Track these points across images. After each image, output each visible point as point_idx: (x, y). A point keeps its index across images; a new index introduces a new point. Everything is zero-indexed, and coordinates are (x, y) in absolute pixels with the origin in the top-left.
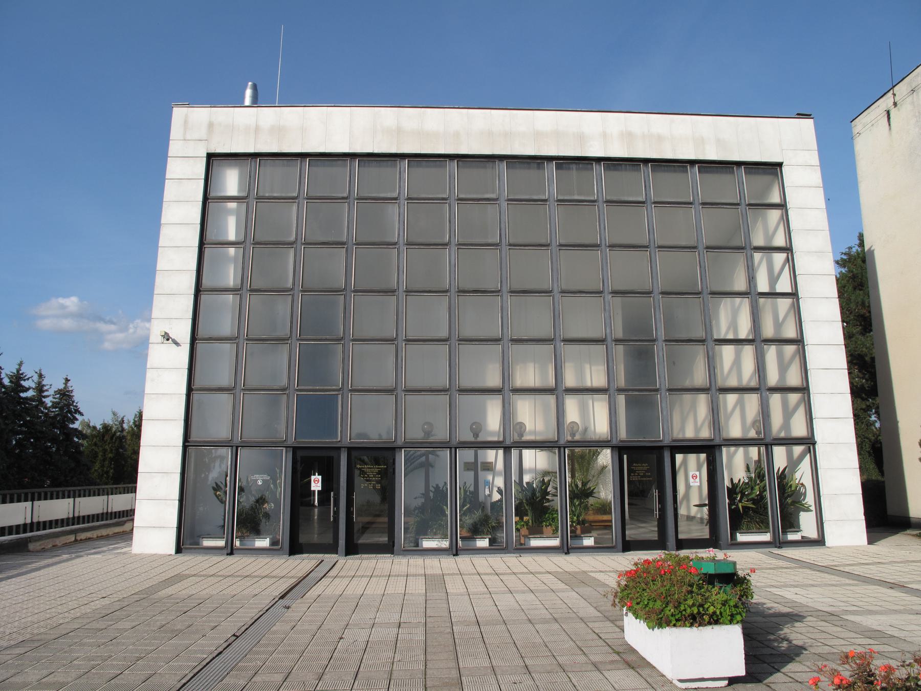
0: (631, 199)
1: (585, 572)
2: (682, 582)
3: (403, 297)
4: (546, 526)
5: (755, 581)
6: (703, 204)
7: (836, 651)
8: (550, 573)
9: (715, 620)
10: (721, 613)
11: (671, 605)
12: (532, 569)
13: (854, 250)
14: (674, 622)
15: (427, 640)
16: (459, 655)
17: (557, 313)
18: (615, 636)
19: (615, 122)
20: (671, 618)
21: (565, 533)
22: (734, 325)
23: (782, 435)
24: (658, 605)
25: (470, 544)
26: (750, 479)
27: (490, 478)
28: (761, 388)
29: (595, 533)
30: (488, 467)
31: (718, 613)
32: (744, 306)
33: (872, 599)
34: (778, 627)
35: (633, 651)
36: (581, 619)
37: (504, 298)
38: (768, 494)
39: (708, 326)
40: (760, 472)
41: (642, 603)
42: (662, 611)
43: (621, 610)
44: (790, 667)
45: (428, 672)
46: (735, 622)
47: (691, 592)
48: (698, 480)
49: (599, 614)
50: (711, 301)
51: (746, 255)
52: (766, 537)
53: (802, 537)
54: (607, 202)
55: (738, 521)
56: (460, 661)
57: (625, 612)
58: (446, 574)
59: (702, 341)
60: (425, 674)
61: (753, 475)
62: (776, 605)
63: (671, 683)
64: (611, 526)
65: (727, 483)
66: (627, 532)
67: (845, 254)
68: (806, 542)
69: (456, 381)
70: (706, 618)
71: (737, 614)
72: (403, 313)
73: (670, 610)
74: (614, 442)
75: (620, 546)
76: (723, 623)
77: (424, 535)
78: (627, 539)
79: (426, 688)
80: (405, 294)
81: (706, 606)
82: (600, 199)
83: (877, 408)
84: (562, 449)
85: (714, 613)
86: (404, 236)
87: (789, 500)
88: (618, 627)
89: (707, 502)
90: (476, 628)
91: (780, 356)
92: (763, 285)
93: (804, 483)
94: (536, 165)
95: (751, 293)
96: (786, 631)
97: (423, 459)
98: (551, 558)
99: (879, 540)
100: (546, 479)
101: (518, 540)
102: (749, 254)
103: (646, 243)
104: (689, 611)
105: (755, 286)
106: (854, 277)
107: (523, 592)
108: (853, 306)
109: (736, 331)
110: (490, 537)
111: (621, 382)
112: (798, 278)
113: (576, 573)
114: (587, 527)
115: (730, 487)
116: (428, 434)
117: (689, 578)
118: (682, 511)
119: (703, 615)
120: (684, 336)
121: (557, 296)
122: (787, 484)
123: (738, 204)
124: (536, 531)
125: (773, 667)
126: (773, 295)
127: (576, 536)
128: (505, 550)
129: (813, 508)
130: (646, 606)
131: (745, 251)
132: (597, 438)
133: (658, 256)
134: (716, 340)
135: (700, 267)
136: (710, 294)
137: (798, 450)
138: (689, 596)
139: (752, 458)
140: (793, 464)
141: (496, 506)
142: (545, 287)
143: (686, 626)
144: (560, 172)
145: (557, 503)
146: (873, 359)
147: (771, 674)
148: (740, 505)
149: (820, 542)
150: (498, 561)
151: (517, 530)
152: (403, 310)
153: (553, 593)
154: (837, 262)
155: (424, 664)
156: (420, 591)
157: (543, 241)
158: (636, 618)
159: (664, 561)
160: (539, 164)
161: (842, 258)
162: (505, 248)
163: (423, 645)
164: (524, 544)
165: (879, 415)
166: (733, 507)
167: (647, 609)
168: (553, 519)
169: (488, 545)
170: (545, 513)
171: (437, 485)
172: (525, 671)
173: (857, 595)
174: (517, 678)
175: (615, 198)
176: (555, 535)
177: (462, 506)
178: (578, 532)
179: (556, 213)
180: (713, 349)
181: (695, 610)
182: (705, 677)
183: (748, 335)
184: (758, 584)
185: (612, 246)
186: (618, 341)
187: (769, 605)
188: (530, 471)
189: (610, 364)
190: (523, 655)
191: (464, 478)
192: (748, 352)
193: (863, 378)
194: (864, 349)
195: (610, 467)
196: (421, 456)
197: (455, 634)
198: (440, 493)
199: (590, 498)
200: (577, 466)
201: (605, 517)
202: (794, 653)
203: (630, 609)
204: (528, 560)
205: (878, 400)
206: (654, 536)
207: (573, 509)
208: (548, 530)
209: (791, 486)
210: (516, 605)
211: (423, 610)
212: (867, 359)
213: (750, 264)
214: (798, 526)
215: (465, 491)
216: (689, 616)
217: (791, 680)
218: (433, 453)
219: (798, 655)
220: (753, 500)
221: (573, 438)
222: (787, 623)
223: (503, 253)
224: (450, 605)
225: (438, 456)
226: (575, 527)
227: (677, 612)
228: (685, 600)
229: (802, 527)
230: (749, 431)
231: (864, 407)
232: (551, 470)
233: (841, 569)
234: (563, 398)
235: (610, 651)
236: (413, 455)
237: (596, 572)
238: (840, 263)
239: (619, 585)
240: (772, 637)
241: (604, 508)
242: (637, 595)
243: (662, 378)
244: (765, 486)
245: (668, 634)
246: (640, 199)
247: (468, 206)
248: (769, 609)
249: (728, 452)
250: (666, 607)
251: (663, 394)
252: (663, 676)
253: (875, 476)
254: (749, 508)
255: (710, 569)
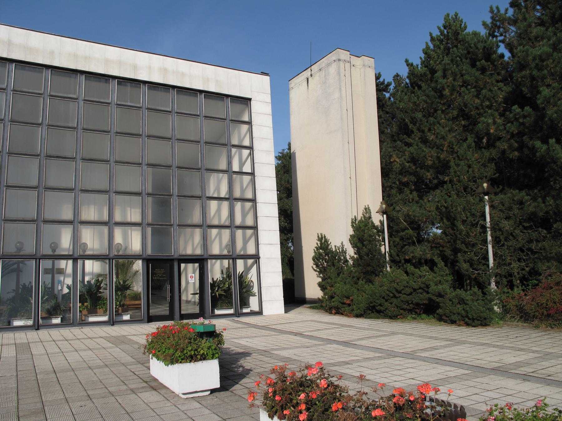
0: (163, 109)
1: (124, 336)
2: (185, 337)
3: (6, 158)
4: (100, 308)
5: (226, 336)
6: (205, 117)
7: (267, 370)
8: (102, 337)
9: (204, 358)
10: (207, 354)
11: (179, 350)
12: (89, 335)
13: (285, 151)
14: (180, 360)
15: (19, 387)
16: (42, 394)
17: (112, 175)
18: (144, 372)
19: (157, 61)
20: (179, 358)
21: (112, 313)
22: (218, 189)
23: (242, 253)
24: (171, 351)
25: (47, 322)
26: (223, 278)
27: (62, 278)
28: (231, 226)
29: (130, 312)
30: (61, 272)
31: (205, 353)
32: (225, 179)
33: (286, 342)
34: (237, 360)
35: (156, 380)
36: (123, 364)
37: (78, 163)
38: (233, 287)
39: (203, 188)
40: (229, 274)
41: (161, 351)
42: (174, 354)
43: (149, 356)
44: (244, 381)
45: (20, 407)
46: (215, 358)
47: (190, 343)
48: (193, 279)
49: (134, 360)
50: (206, 174)
51: (228, 149)
52: (231, 311)
53: (251, 310)
54: (148, 109)
55: (215, 303)
56: (43, 397)
57: (151, 357)
58: (31, 342)
59: (199, 197)
60: (18, 409)
61: (225, 276)
62: (236, 348)
63: (178, 396)
64: (141, 308)
65: (210, 281)
66: (150, 311)
67: (281, 153)
68: (253, 313)
69: (42, 215)
70: (199, 357)
71: (216, 353)
72: (5, 168)
73: (178, 353)
74: (144, 256)
75: (146, 319)
76: (208, 359)
77: (14, 317)
78: (150, 315)
79: (19, 417)
80: (7, 155)
81: (199, 350)
82: (144, 106)
83: (293, 239)
84: (111, 260)
85: (203, 354)
86: (9, 115)
87: (244, 290)
88: (146, 367)
89: (198, 292)
90: (54, 375)
91: (243, 208)
92: (236, 168)
93: (253, 281)
94: (104, 80)
95: (228, 171)
96: (242, 362)
97: (15, 266)
98: (102, 328)
99: (290, 310)
100: (100, 279)
101: (81, 319)
102: (229, 149)
103: (170, 136)
104: (189, 353)
105: (232, 167)
106: (284, 166)
107: (85, 350)
108: (283, 182)
109: (219, 193)
110: (62, 316)
111: (150, 219)
112: (255, 165)
113: (119, 336)
114: (125, 309)
115: (212, 283)
116: (20, 249)
117: (189, 335)
118: (184, 298)
119: (197, 355)
120: (189, 194)
121: (113, 164)
122: (244, 281)
123: (225, 119)
124: (93, 311)
125: (235, 382)
126: (241, 173)
127: (119, 314)
128: (72, 324)
129: (257, 294)
130: (164, 352)
131: (227, 147)
132: (133, 253)
133: (177, 145)
134: (208, 197)
135: (201, 154)
136: (206, 170)
137: (250, 261)
138: (189, 345)
139: (224, 266)
140: (247, 269)
141: (66, 297)
142: (105, 158)
143: (187, 362)
144: (118, 86)
145: (106, 293)
146: (292, 212)
147: (234, 386)
148: (217, 293)
149: (260, 313)
150: (66, 332)
151: (80, 311)
152: (5, 166)
153: (104, 350)
154: (276, 157)
155: (17, 402)
156: (12, 355)
157: (106, 129)
158: (158, 360)
159: (174, 326)
160: (106, 79)
161: (279, 155)
162: (80, 131)
163: (16, 390)
164: (85, 320)
165: (293, 243)
166: (213, 294)
167: (165, 354)
168: (104, 304)
169: (60, 322)
170: (99, 300)
171: (24, 284)
172: (88, 398)
173: (279, 340)
174: (82, 403)
175: (153, 107)
176: (105, 314)
177: (42, 298)
178: (120, 311)
179: (115, 112)
180: (206, 202)
181: (193, 353)
182: (198, 390)
183: (226, 195)
184: (227, 337)
185: (149, 136)
186: (149, 194)
187: (232, 349)
188: (89, 274)
189: (144, 209)
190: (86, 389)
191: (45, 279)
192: (225, 205)
193: (286, 222)
194: (287, 207)
195: (141, 271)
196: (15, 263)
197: (39, 380)
198: (27, 290)
199: (128, 290)
200: (120, 271)
201: (137, 302)
202: (246, 373)
203: (154, 355)
204: (87, 330)
205: (293, 235)
206: (167, 313)
207: (117, 297)
208: (100, 311)
209: (245, 282)
210: (80, 358)
211: (15, 367)
212: (289, 212)
213: (229, 154)
214: (249, 305)
215: (45, 288)
216: (189, 356)
217: (244, 387)
218: (22, 262)
219: (248, 374)
220: (224, 290)
221: (118, 253)
222: (242, 358)
223: (79, 134)
224: (35, 362)
225: (25, 264)
226: (118, 308)
227: (182, 354)
228: (187, 347)
229: (251, 305)
230: (224, 250)
231: (286, 238)
232: (102, 273)
233: (271, 327)
234: (113, 228)
235: (141, 381)
236: (7, 264)
237: (131, 335)
238: (278, 158)
239: (148, 341)
240: (234, 366)
241: (137, 297)
242: (159, 346)
243: (175, 218)
244: (232, 282)
245: (177, 367)
246: (168, 110)
247: (57, 101)
248: (232, 351)
249: (211, 263)
250: (176, 352)
251: (175, 228)
252: (173, 392)
253: (290, 276)
254: (222, 295)
255: (201, 329)
